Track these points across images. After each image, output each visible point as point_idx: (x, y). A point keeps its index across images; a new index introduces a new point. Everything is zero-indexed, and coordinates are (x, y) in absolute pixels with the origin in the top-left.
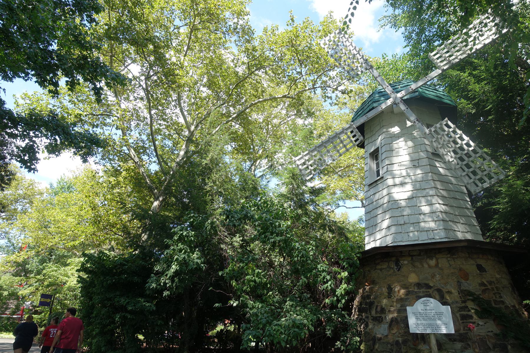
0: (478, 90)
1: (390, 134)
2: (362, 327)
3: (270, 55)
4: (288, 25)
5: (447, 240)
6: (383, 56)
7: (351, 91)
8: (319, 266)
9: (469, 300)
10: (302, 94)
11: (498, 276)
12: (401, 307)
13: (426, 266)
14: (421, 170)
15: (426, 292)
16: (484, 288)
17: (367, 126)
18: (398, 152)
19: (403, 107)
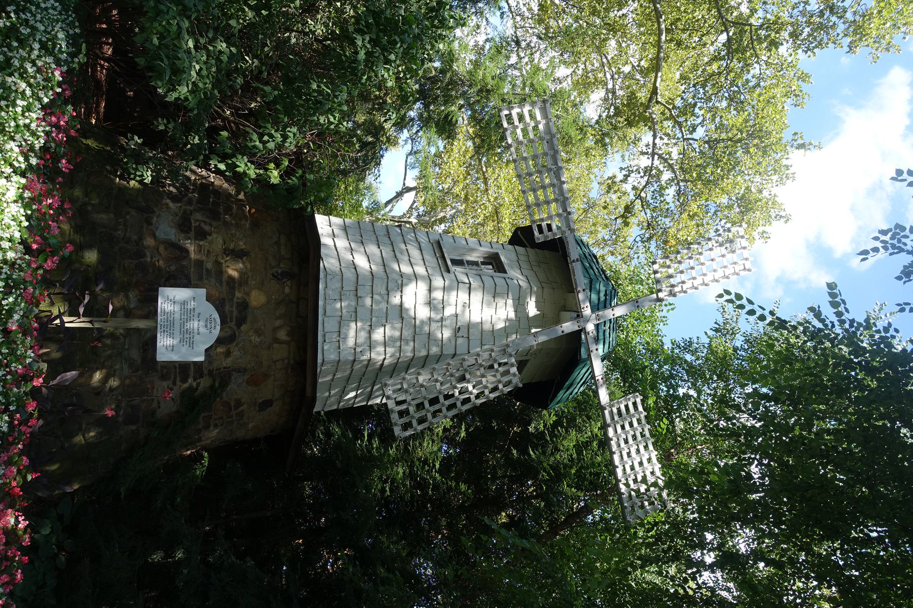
0: (565, 443)
1: (526, 298)
2: (171, 189)
3: (749, 77)
4: (795, 134)
5: (319, 361)
6: (671, 304)
7: (626, 224)
8: (295, 129)
9: (214, 381)
10: (650, 128)
11: (251, 426)
12: (207, 270)
13: (278, 323)
14: (449, 339)
15: (231, 318)
16: (233, 404)
17: (550, 257)
18: (489, 304)
19: (568, 327)
